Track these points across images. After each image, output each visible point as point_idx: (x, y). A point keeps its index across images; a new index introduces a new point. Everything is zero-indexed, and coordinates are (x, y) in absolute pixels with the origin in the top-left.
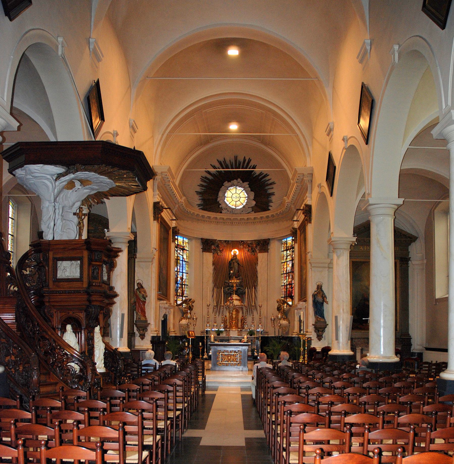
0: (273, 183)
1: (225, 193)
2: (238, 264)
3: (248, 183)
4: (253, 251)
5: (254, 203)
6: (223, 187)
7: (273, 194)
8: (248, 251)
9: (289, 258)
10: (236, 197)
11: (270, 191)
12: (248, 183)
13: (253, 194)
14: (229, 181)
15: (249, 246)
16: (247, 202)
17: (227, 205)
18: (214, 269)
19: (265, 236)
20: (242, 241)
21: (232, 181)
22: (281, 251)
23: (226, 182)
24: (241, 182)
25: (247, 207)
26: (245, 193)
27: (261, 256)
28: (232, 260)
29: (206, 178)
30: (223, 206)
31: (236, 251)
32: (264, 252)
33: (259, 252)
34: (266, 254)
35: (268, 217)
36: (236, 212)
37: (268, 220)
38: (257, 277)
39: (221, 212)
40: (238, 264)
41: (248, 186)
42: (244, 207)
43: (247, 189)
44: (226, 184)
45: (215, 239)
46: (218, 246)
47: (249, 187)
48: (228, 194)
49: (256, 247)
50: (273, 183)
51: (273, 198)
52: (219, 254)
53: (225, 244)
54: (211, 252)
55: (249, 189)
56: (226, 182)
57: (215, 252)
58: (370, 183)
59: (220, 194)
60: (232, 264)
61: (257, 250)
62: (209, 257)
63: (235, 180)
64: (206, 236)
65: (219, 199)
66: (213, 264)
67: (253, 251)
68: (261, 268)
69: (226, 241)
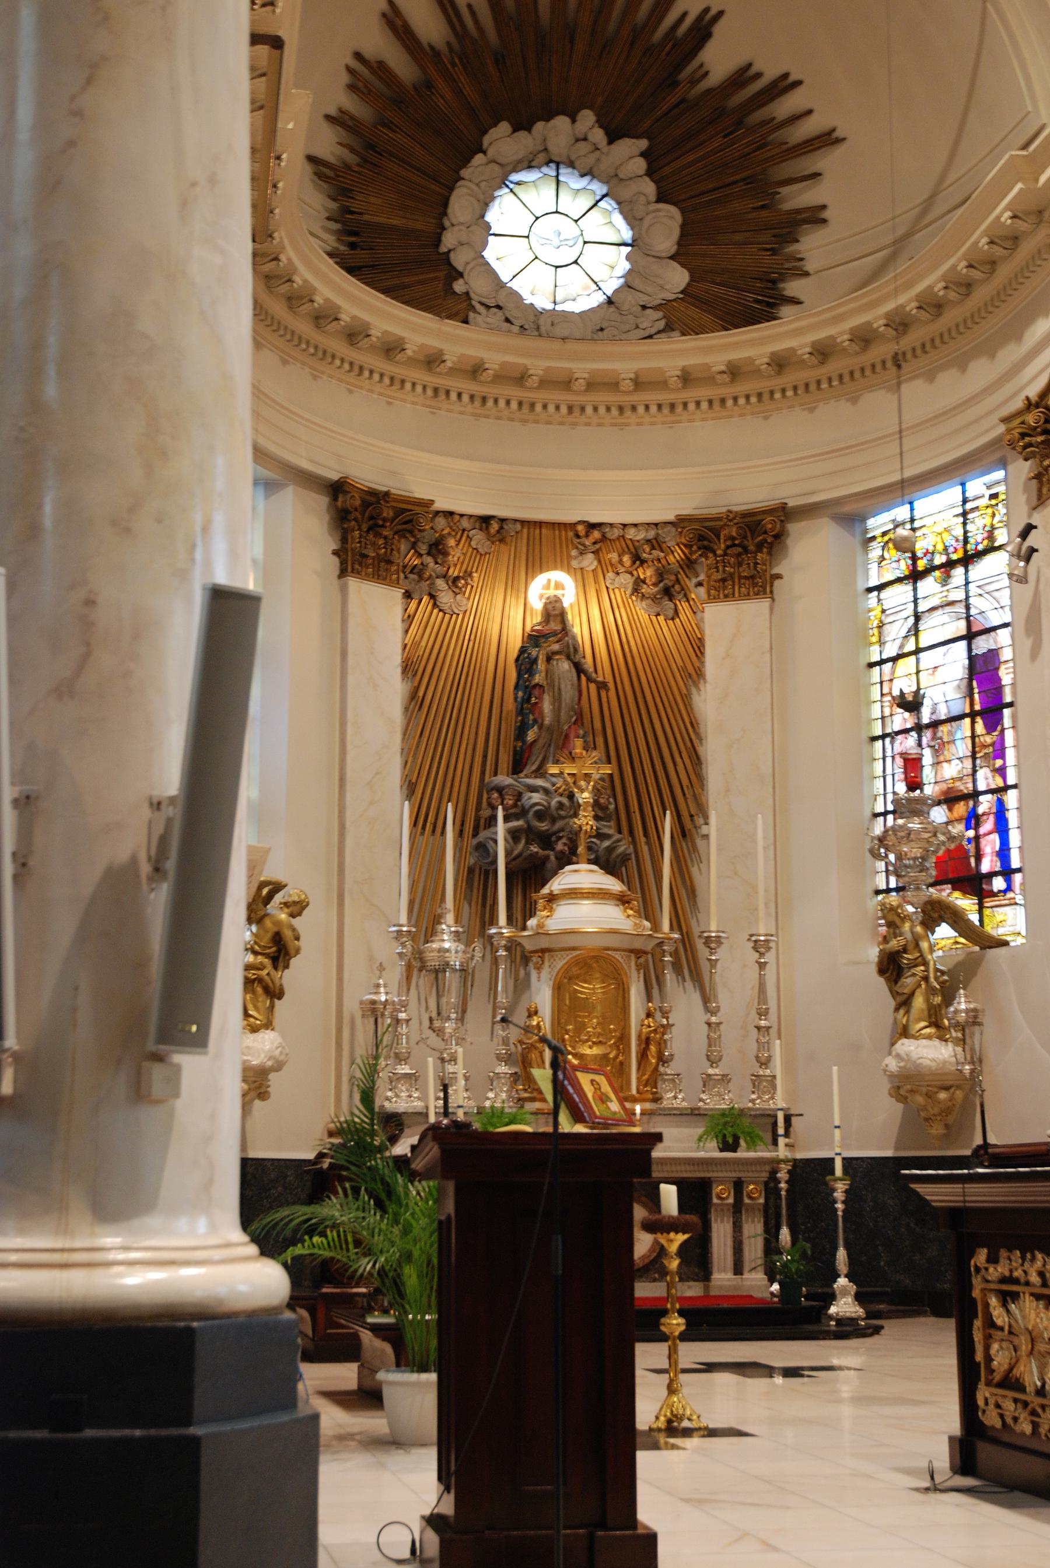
0: (828, 139)
1: (486, 204)
2: (579, 668)
3: (643, 144)
4: (668, 591)
5: (678, 278)
6: (479, 158)
7: (815, 216)
8: (639, 583)
9: (942, 626)
10: (555, 238)
11: (798, 198)
12: (643, 144)
13: (668, 223)
14: (522, 125)
15: (638, 559)
16: (627, 275)
17: (501, 285)
18: (413, 695)
19: (750, 489)
20: (592, 526)
21: (539, 126)
22: (862, 586)
23: (504, 127)
24: (598, 136)
25: (631, 300)
26: (618, 219)
27: (728, 626)
28: (534, 639)
29: (380, 68)
30: (474, 285)
31: (554, 585)
32: (747, 596)
33: (712, 598)
34: (764, 605)
35: (780, 363)
36: (560, 330)
37: (790, 382)
38: (697, 761)
39: (466, 321)
40: (579, 668)
41: (640, 165)
42: (610, 301)
43: (627, 192)
44: (501, 140)
45: (420, 492)
46: (438, 549)
47: (649, 173)
48: (505, 212)
49: (689, 564)
50: (828, 139)
51: (813, 247)
52: (445, 598)
53: (478, 537)
54: (396, 584)
55: (649, 188)
56: (504, 127)
57: (416, 585)
58: (448, 784)
59: (459, 206)
60: (541, 665)
61: (691, 584)
62: (379, 609)
63: (562, 122)
64: (369, 471)
65: (449, 240)
66: (408, 668)
67: (668, 593)
68: (723, 709)
69: (485, 521)
